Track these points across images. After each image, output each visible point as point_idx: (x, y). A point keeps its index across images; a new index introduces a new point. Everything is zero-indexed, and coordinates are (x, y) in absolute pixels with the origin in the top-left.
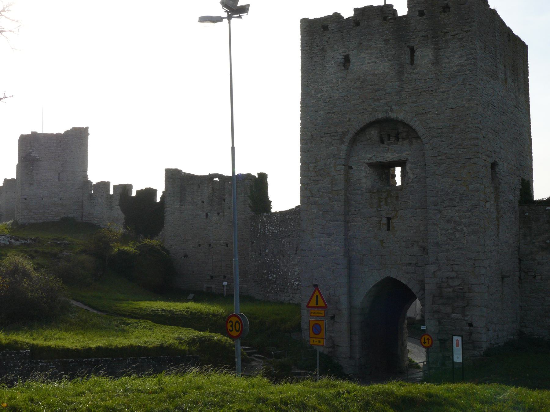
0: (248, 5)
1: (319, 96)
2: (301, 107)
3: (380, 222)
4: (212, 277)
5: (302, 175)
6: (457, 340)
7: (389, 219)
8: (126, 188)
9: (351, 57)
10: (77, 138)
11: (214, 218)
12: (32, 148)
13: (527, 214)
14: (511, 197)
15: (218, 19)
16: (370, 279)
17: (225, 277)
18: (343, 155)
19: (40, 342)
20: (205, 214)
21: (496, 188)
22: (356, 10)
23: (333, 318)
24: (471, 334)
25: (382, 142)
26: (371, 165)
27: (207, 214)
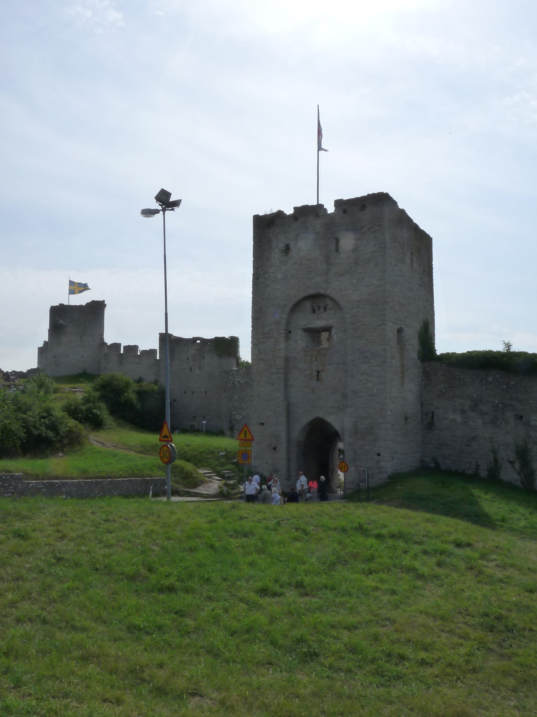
0: (180, 201)
1: (266, 276)
2: (253, 285)
3: (312, 374)
4: (194, 417)
5: (253, 337)
7: (318, 372)
8: (135, 348)
11: (197, 371)
12: (60, 315)
13: (428, 369)
15: (157, 211)
16: (303, 419)
17: (204, 417)
18: (284, 322)
20: (189, 369)
22: (295, 208)
24: (378, 462)
27: (191, 369)
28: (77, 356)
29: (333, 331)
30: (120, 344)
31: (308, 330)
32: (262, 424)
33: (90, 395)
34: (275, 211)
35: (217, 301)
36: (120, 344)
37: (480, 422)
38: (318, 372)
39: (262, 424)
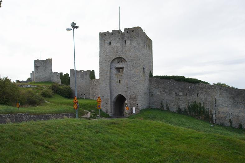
4: (81, 95)
6: (134, 108)
7: (120, 81)
9: (111, 42)
10: (49, 61)
12: (38, 64)
14: (148, 76)
15: (71, 29)
16: (116, 94)
18: (109, 65)
19: (30, 110)
21: (144, 74)
22: (112, 31)
23: (107, 103)
24: (137, 107)
25: (118, 63)
26: (116, 68)
28: (43, 75)
29: (124, 68)
30: (57, 72)
31: (117, 68)
32: (103, 96)
33: (107, 112)
34: (106, 31)
35: (89, 59)
36: (57, 72)
37: (165, 95)
38: (120, 81)
39: (103, 96)
